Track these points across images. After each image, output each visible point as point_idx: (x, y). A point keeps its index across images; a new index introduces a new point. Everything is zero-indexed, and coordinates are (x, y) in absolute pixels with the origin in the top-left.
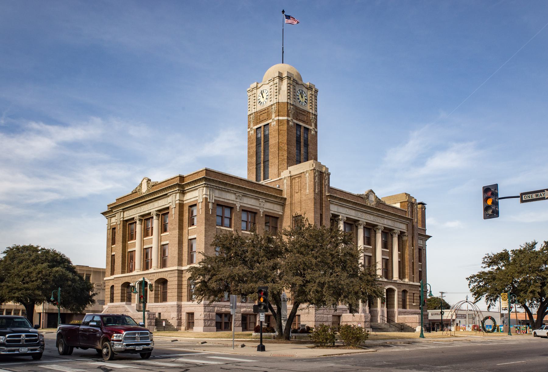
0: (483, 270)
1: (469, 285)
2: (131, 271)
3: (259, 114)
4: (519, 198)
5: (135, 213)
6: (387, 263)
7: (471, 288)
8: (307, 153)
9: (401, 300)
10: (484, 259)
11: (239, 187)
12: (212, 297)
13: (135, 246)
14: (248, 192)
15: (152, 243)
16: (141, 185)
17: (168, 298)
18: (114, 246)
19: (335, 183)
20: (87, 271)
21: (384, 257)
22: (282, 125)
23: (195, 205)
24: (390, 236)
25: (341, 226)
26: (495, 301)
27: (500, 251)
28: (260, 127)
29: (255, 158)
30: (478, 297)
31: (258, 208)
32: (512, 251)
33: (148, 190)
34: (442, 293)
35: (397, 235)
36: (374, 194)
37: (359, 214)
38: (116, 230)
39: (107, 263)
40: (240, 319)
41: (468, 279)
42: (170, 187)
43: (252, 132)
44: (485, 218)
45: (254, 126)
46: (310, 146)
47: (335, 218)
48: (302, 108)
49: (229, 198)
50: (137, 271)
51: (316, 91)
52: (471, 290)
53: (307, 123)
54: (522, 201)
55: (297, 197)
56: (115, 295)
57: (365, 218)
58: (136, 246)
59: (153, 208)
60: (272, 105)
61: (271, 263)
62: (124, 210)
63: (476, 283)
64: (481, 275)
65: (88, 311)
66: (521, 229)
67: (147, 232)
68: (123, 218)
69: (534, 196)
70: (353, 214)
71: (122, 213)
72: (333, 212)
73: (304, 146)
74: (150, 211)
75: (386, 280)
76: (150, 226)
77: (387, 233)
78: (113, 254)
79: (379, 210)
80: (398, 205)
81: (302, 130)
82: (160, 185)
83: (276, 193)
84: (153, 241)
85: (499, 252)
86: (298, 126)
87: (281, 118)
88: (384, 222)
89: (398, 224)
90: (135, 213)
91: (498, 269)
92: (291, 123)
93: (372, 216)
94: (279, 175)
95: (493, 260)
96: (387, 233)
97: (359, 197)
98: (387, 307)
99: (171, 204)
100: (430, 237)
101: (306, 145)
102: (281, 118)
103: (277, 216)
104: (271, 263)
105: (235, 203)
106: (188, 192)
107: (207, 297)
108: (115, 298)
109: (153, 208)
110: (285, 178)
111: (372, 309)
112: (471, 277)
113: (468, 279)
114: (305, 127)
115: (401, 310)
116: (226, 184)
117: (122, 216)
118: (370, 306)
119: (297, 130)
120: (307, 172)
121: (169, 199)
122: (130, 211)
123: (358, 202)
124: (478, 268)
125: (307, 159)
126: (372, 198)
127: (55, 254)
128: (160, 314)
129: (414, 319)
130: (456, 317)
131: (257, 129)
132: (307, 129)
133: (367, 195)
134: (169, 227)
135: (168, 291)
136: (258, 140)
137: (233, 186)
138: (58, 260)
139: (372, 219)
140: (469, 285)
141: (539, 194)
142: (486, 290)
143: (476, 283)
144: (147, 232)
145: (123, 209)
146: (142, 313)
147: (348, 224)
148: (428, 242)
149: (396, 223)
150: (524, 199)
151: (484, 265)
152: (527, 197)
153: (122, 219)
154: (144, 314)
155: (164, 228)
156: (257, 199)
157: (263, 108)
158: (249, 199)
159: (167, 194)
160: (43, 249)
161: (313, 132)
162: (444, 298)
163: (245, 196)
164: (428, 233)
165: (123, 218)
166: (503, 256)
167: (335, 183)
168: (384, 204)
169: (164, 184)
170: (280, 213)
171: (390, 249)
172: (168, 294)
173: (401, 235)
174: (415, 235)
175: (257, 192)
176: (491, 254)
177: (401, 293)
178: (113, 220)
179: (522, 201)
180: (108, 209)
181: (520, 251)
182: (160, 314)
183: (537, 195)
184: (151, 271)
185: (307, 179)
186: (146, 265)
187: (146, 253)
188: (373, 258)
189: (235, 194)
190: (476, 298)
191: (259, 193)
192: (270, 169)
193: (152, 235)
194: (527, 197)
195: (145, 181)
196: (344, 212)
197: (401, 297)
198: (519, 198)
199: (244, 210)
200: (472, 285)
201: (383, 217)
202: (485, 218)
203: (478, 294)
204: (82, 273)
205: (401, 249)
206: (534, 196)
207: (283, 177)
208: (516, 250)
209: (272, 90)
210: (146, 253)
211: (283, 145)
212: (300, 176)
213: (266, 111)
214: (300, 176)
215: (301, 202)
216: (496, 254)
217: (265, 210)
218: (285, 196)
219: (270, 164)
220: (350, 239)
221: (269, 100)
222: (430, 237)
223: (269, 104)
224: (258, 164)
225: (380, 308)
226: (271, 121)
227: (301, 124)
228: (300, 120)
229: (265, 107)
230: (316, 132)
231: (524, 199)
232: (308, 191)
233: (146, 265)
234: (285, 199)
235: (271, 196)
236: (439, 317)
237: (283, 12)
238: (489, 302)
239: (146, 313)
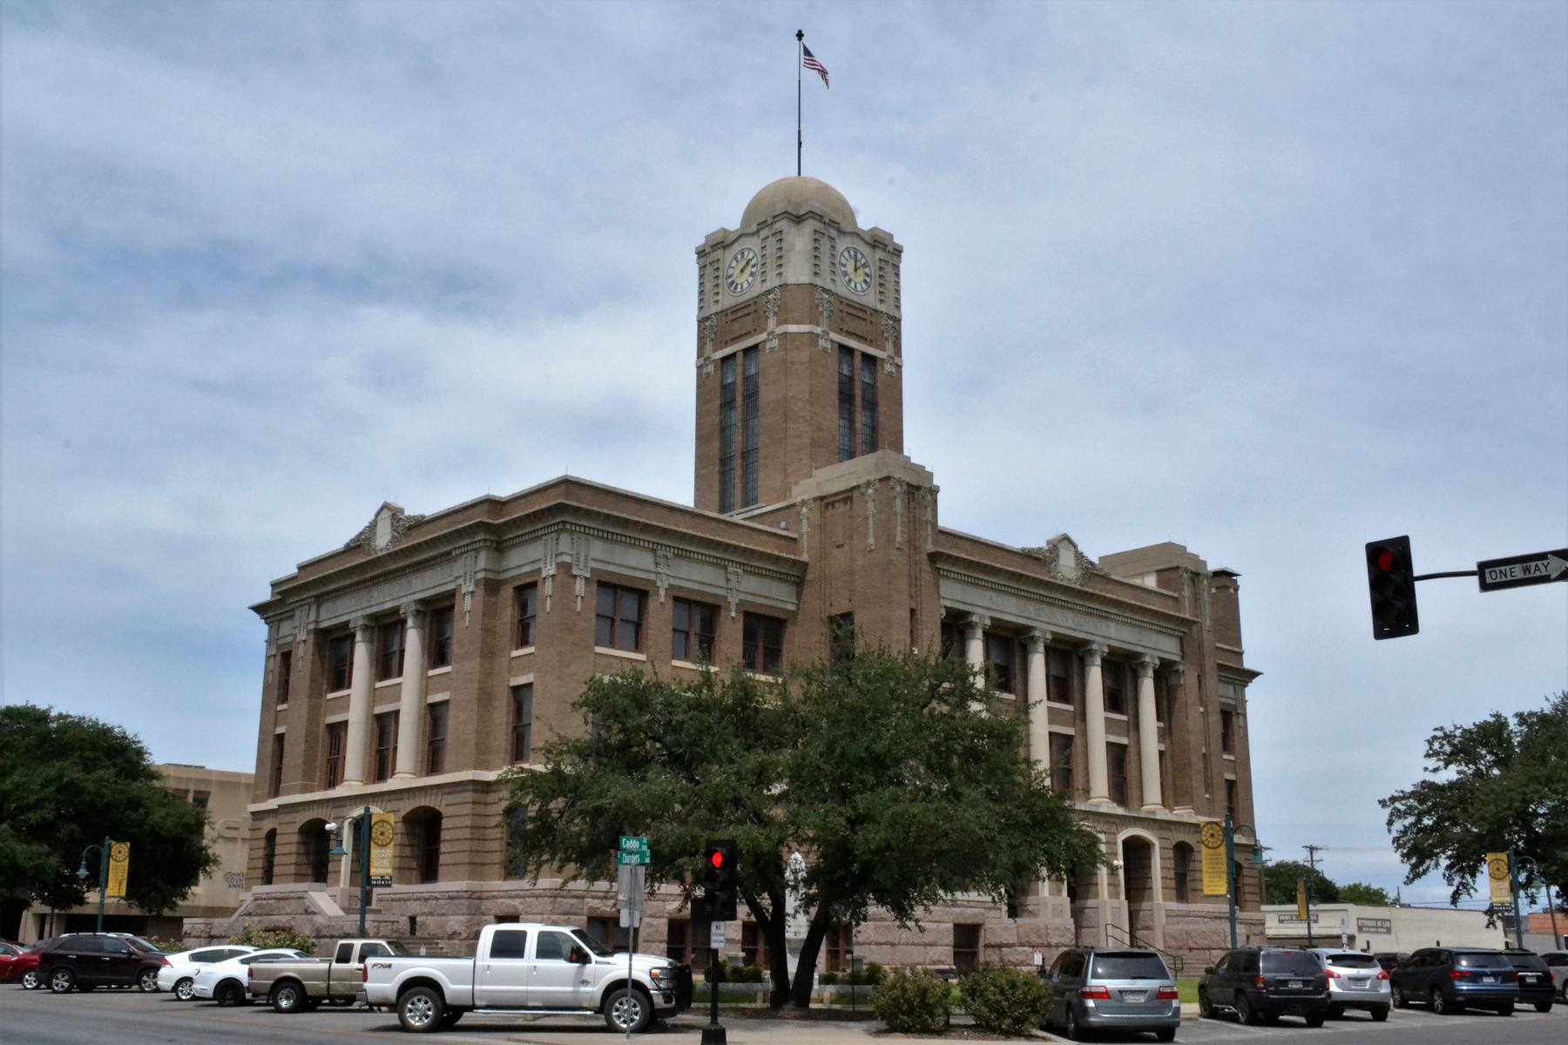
0: (1431, 777)
1: (1390, 823)
2: (332, 784)
3: (730, 318)
4: (1476, 578)
5: (352, 610)
6: (1119, 757)
7: (1395, 834)
8: (874, 428)
9: (1172, 874)
10: (1430, 743)
11: (664, 532)
12: (571, 868)
13: (346, 708)
14: (690, 543)
15: (398, 699)
16: (373, 526)
17: (441, 870)
18: (284, 706)
19: (953, 514)
20: (198, 781)
21: (1113, 739)
22: (798, 348)
23: (534, 585)
24: (1129, 676)
25: (976, 653)
26: (1473, 875)
27: (1484, 716)
28: (733, 356)
29: (716, 444)
30: (1420, 863)
31: (723, 592)
32: (1520, 716)
33: (394, 540)
34: (1312, 849)
35: (1150, 673)
36: (1075, 546)
37: (1031, 609)
38: (293, 660)
39: (260, 761)
40: (665, 936)
41: (1383, 803)
42: (460, 534)
43: (711, 368)
44: (1380, 634)
45: (715, 350)
46: (882, 408)
47: (956, 626)
48: (854, 298)
49: (634, 563)
50: (353, 783)
51: (898, 252)
52: (1396, 840)
53: (871, 342)
54: (1485, 587)
55: (838, 557)
56: (277, 860)
57: (1049, 621)
58: (355, 706)
59: (404, 595)
60: (769, 292)
61: (753, 759)
62: (320, 600)
63: (1411, 820)
64: (1427, 792)
65: (194, 912)
66: (1497, 660)
67: (387, 664)
68: (317, 622)
69: (1518, 572)
70: (1012, 610)
71: (314, 609)
72: (948, 604)
73: (864, 408)
74: (396, 603)
75: (1120, 811)
76: (396, 648)
77: (1121, 668)
78: (280, 730)
79: (1091, 597)
80: (1150, 582)
81: (858, 360)
82: (430, 526)
83: (778, 547)
84: (408, 694)
85: (1479, 720)
86: (846, 351)
87: (792, 328)
88: (1108, 634)
89: (1154, 636)
90: (352, 610)
91: (1478, 774)
92: (822, 342)
93: (1070, 615)
94: (785, 492)
95: (1463, 746)
96: (1121, 668)
97: (1028, 556)
98: (1128, 897)
99: (460, 581)
100: (1253, 675)
101: (871, 406)
102: (792, 328)
103: (782, 616)
104: (753, 759)
105: (652, 577)
106: (515, 546)
107: (556, 864)
108: (276, 870)
109: (404, 595)
110: (803, 503)
111: (1079, 903)
112: (1393, 799)
113: (1383, 803)
114: (865, 356)
115: (1174, 906)
116: (626, 523)
117: (312, 618)
118: (1073, 894)
119: (840, 363)
120: (868, 484)
121: (458, 568)
122: (340, 602)
123: (1025, 571)
124: (1413, 767)
125: (873, 446)
126: (1066, 562)
127: (105, 732)
128: (413, 920)
129: (1215, 938)
130: (1360, 929)
131: (724, 360)
132: (870, 360)
133: (1054, 546)
134: (455, 648)
135: (444, 848)
136: (727, 389)
137: (646, 528)
138: (113, 752)
139: (1071, 624)
140: (1390, 823)
141: (1533, 564)
142: (1443, 844)
143: (1411, 820)
144: (387, 664)
145: (317, 597)
146: (357, 917)
147: (995, 637)
148: (1252, 691)
149: (1145, 633)
150: (1489, 581)
151: (1432, 763)
152: (1494, 575)
153: (312, 626)
154: (363, 920)
155: (438, 653)
156: (720, 565)
157: (741, 300)
158: (696, 566)
159: (449, 553)
160: (60, 716)
161: (888, 367)
162: (1318, 867)
163: (682, 555)
164: (1248, 663)
165: (317, 622)
166: (1491, 733)
167: (953, 514)
168: (1106, 579)
169: (444, 522)
170: (792, 607)
171: (1131, 712)
172: (443, 859)
173: (1165, 673)
174: (1208, 669)
175: (718, 545)
176: (1449, 728)
177: (1171, 854)
178: (286, 628)
179: (1485, 587)
180: (273, 595)
181: (1543, 719)
182: (413, 920)
183: (1526, 570)
184: (391, 784)
185: (871, 505)
186: (381, 765)
187: (383, 727)
188: (1078, 742)
189: (654, 551)
190: (1414, 867)
191: (727, 547)
192: (761, 475)
193: (400, 674)
194: (1494, 575)
195: (386, 513)
196: (987, 605)
197: (1171, 864)
198: (1476, 578)
199: (682, 600)
200: (1398, 825)
201: (1105, 617)
202: (1380, 634)
203: (1418, 852)
204: (183, 787)
205: (1165, 710)
206: (1518, 572)
207: (799, 499)
208: (1531, 714)
209: (768, 252)
210: (383, 727)
211: (800, 404)
212: (850, 498)
213: (750, 310)
214: (847, 496)
215: (851, 573)
216: (1468, 725)
217: (742, 596)
218: (805, 557)
219: (761, 461)
220: (1007, 674)
221: (759, 279)
222: (1253, 675)
223: (758, 289)
224: (725, 462)
225: (1108, 899)
226: (764, 336)
227: (852, 343)
228: (850, 334)
229: (747, 296)
230: (899, 367)
231: (1489, 581)
232: (871, 540)
233: (381, 765)
234: (805, 565)
235: (762, 556)
236: (1300, 930)
237: (800, 35)
238: (1457, 880)
239: (369, 917)
